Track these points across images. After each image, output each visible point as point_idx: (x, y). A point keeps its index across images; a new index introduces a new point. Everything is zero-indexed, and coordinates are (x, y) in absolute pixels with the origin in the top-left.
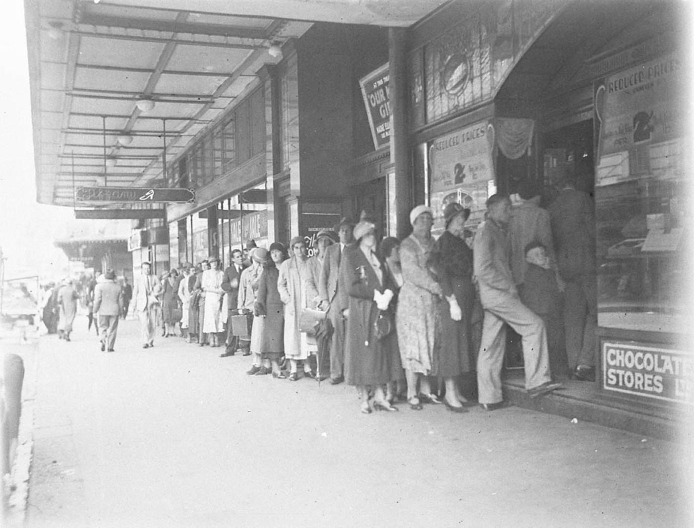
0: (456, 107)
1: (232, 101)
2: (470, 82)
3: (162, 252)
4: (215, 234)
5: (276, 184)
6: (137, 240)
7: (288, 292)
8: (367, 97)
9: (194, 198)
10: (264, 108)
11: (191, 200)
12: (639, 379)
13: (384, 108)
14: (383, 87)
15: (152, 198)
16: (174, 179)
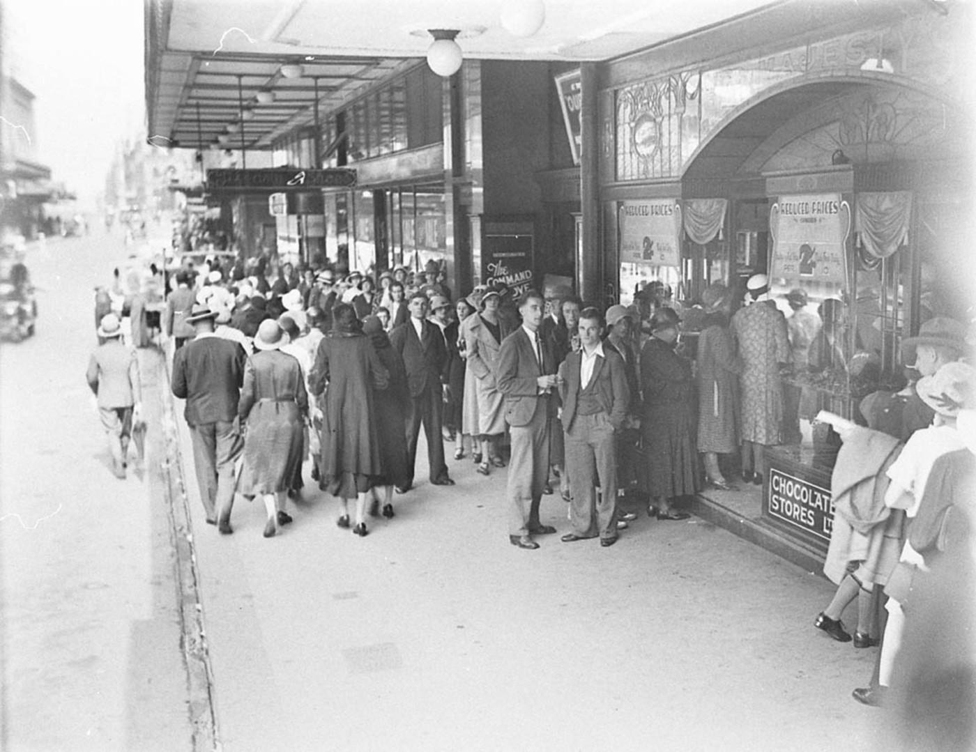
3: (316, 225)
4: (383, 223)
12: (796, 510)
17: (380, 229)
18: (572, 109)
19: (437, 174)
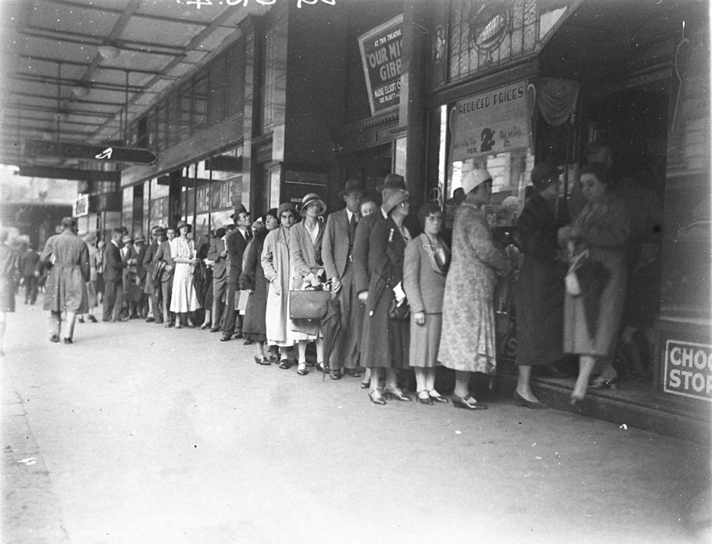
0: (488, 63)
1: (205, 56)
2: (508, 36)
4: (177, 201)
5: (254, 149)
6: (84, 206)
7: (273, 268)
8: (366, 57)
9: (157, 160)
10: (245, 66)
11: (153, 162)
13: (385, 70)
14: (386, 45)
15: (109, 157)
16: (131, 141)
17: (174, 206)
18: (373, 66)
19: (194, 20)
